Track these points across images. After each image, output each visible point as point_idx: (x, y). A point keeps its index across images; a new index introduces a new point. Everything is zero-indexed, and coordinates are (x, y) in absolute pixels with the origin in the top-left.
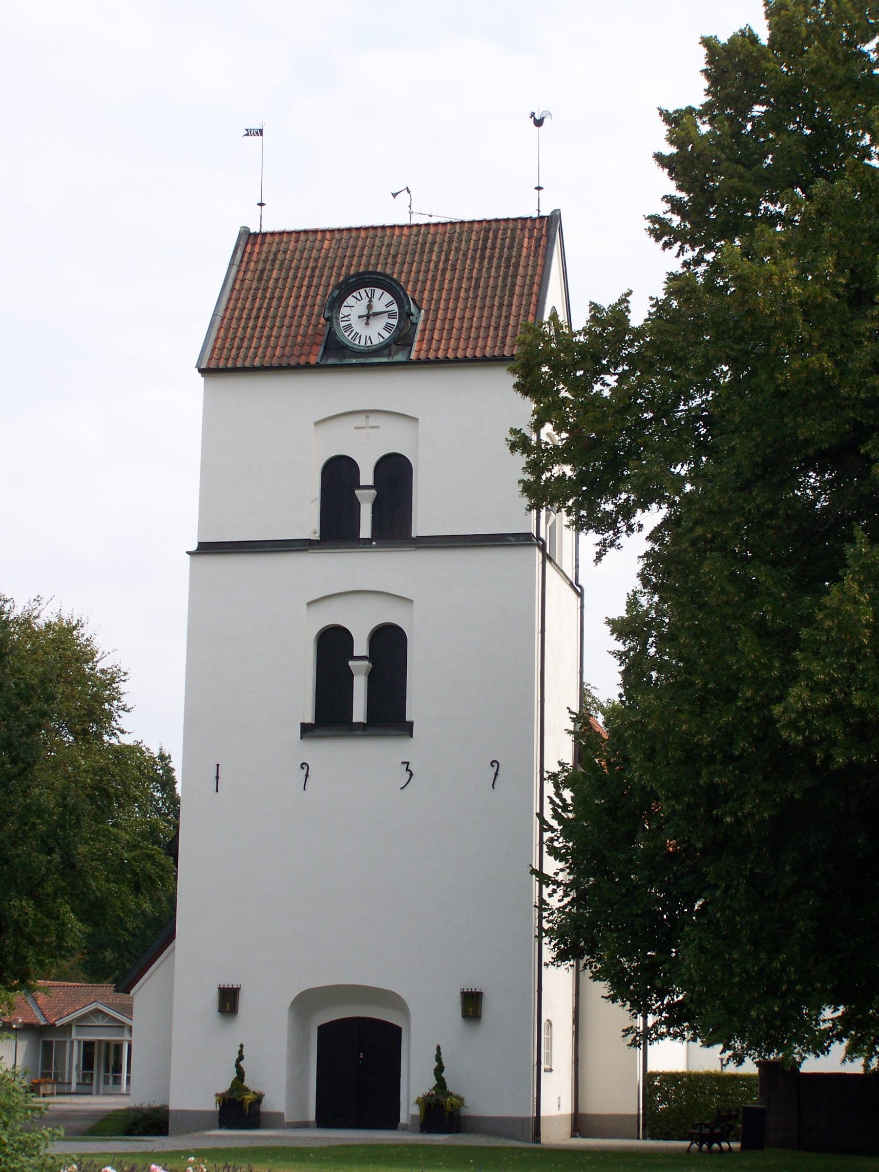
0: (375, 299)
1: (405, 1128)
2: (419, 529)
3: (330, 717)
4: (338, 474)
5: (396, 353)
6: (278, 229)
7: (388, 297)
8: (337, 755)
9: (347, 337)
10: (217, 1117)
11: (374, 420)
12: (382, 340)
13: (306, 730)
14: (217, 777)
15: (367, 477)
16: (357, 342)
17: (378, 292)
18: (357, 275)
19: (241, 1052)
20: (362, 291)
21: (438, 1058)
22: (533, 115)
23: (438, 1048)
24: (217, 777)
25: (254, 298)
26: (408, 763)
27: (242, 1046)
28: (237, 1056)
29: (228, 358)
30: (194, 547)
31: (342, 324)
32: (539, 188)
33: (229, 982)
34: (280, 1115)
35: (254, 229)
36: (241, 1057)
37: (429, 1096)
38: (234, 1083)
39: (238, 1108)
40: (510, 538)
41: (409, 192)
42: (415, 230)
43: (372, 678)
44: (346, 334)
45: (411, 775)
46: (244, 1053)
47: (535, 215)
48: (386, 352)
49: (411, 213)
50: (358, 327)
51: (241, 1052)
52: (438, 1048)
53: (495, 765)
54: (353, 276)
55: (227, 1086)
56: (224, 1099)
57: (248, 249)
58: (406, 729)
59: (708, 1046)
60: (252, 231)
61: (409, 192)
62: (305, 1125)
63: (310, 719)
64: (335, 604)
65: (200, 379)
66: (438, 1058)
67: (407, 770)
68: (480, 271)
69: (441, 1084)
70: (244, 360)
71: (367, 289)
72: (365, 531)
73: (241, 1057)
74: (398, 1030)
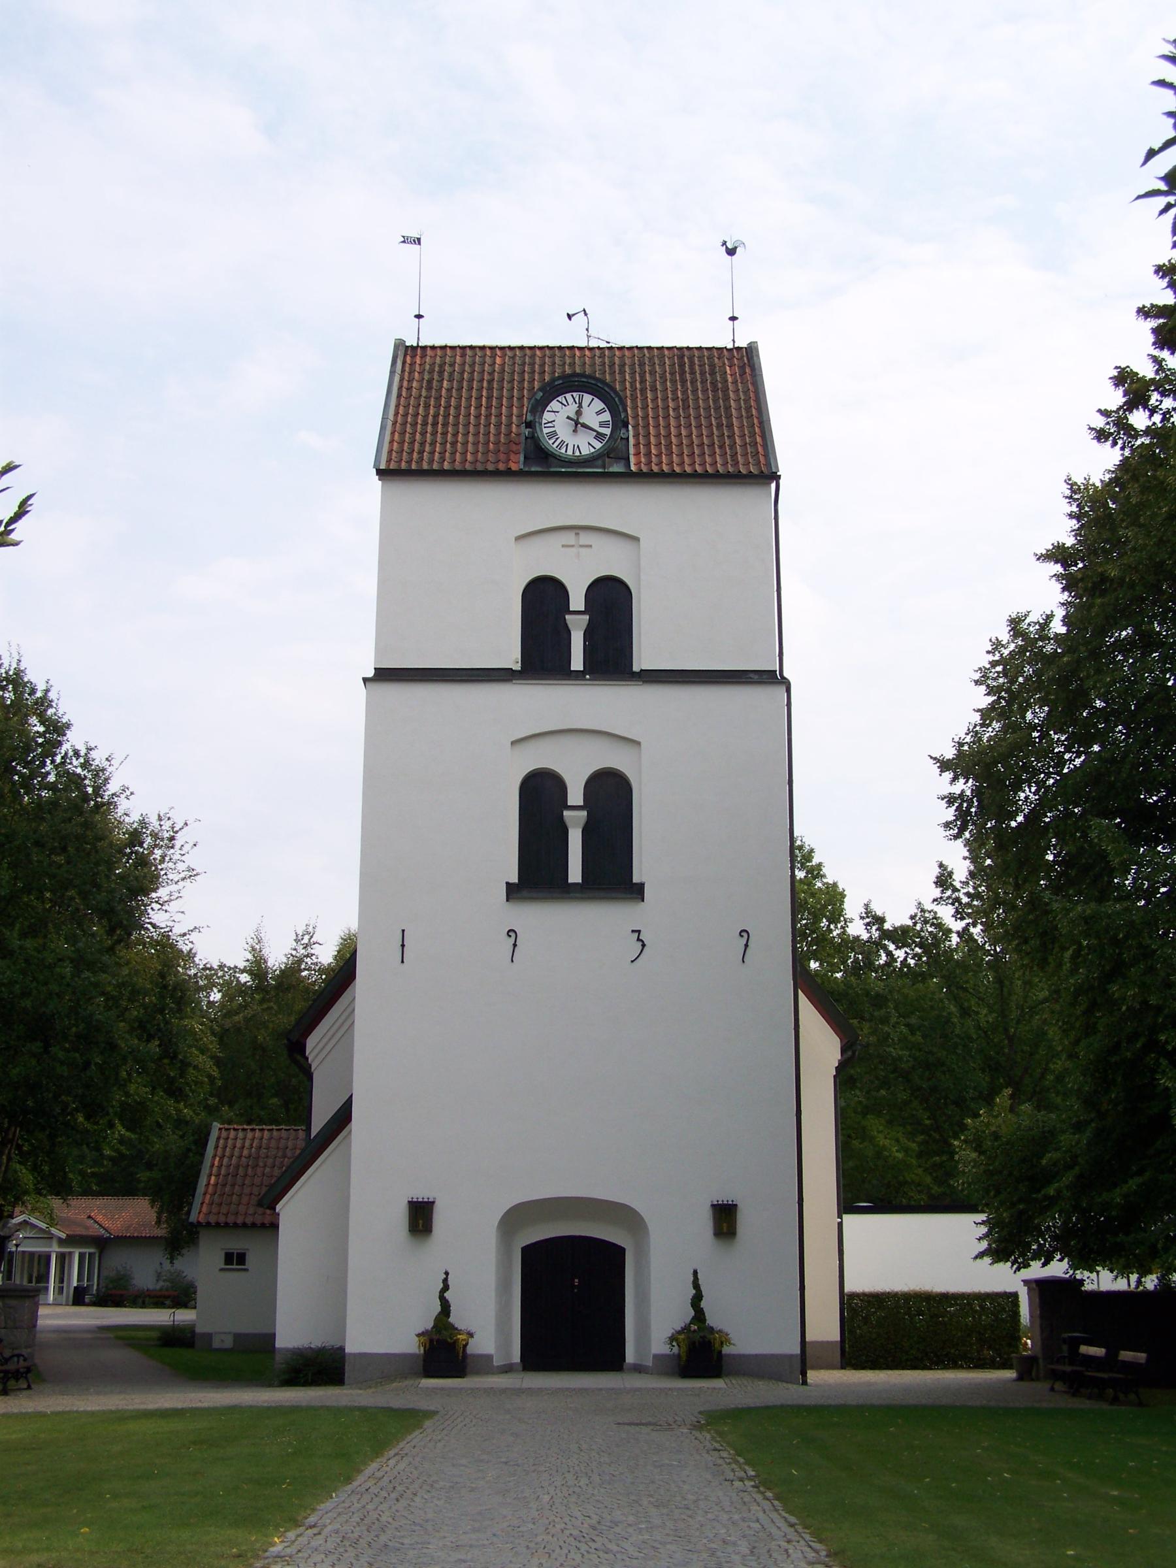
0: (585, 404)
1: (638, 1369)
2: (643, 660)
3: (538, 876)
4: (543, 598)
5: (605, 467)
6: (439, 343)
7: (598, 404)
9: (552, 445)
11: (585, 538)
12: (593, 450)
13: (513, 892)
14: (403, 946)
15: (577, 601)
16: (563, 451)
17: (587, 398)
18: (564, 376)
19: (445, 1281)
20: (568, 396)
21: (696, 1285)
22: (724, 243)
23: (695, 1273)
24: (403, 946)
25: (427, 406)
26: (639, 932)
27: (447, 1273)
28: (441, 1285)
29: (410, 458)
30: (370, 673)
31: (545, 431)
33: (421, 1194)
34: (489, 1357)
35: (411, 341)
36: (446, 1287)
37: (686, 1329)
38: (437, 1320)
39: (443, 1352)
40: (752, 675)
41: (586, 314)
42: (597, 352)
43: (588, 832)
44: (551, 442)
45: (644, 945)
46: (450, 1283)
47: (730, 346)
48: (600, 462)
49: (589, 337)
50: (564, 431)
51: (445, 1281)
52: (695, 1273)
53: (745, 935)
54: (559, 378)
55: (430, 1325)
56: (431, 1341)
57: (408, 359)
58: (637, 892)
59: (431, 1231)
60: (408, 344)
61: (586, 314)
62: (507, 1369)
64: (531, 746)
65: (376, 483)
66: (696, 1285)
67: (638, 939)
68: (685, 392)
69: (699, 1315)
70: (431, 461)
71: (575, 394)
72: (577, 663)
73: (446, 1287)
74: (621, 1251)
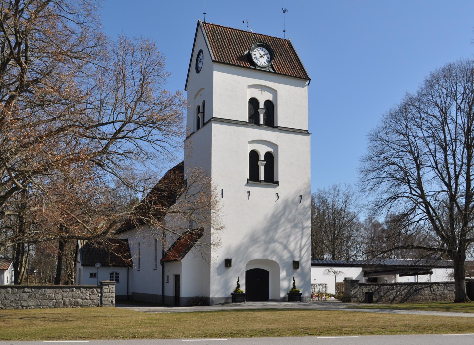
3: (254, 177)
8: (256, 190)
10: (208, 296)
32: (205, 13)
33: (228, 257)
36: (238, 281)
63: (248, 178)
73: (238, 281)
